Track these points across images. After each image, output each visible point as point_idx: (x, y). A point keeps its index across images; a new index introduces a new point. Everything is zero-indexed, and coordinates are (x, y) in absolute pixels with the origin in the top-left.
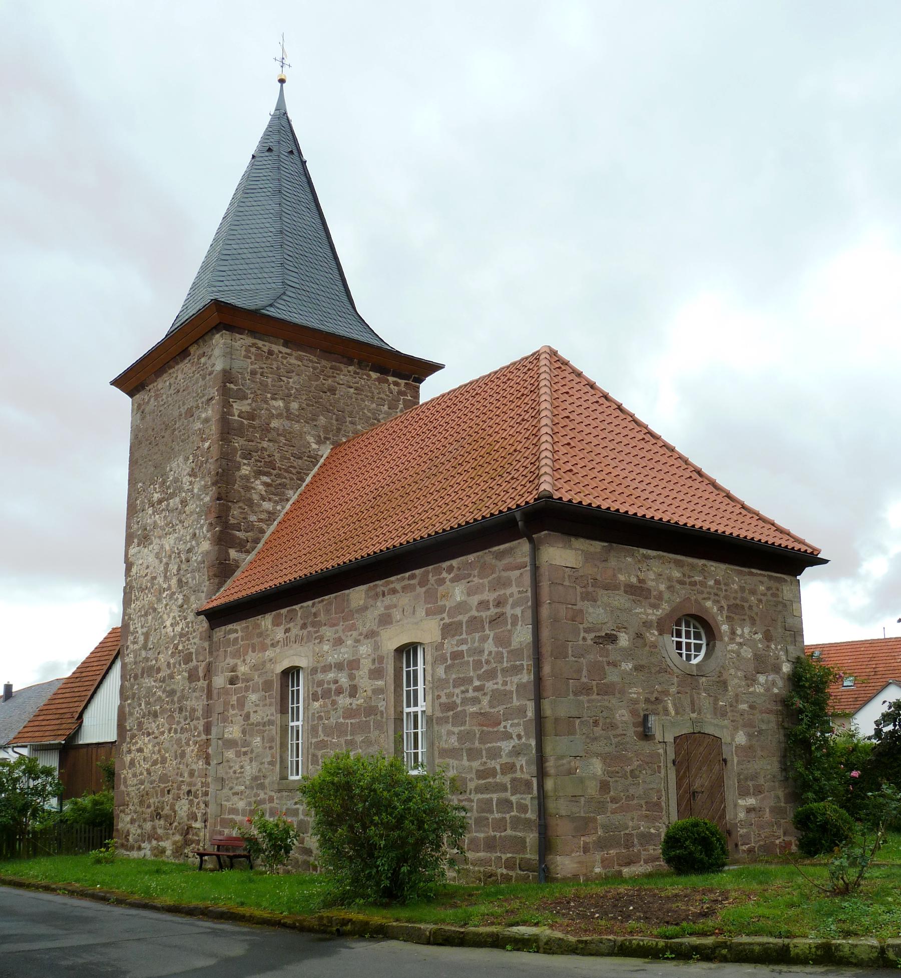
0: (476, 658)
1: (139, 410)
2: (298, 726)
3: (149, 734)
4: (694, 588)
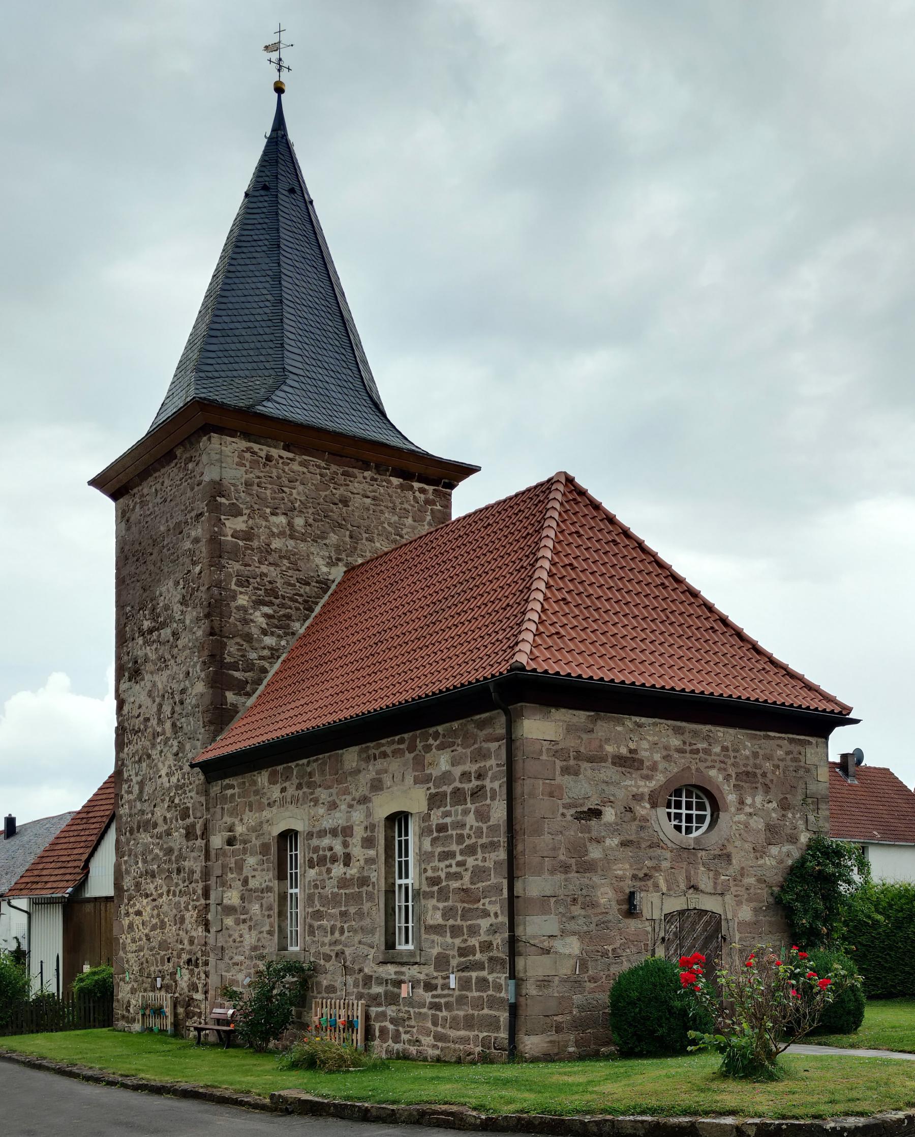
0: (459, 832)
1: (123, 517)
2: (296, 894)
3: (147, 896)
4: (696, 756)
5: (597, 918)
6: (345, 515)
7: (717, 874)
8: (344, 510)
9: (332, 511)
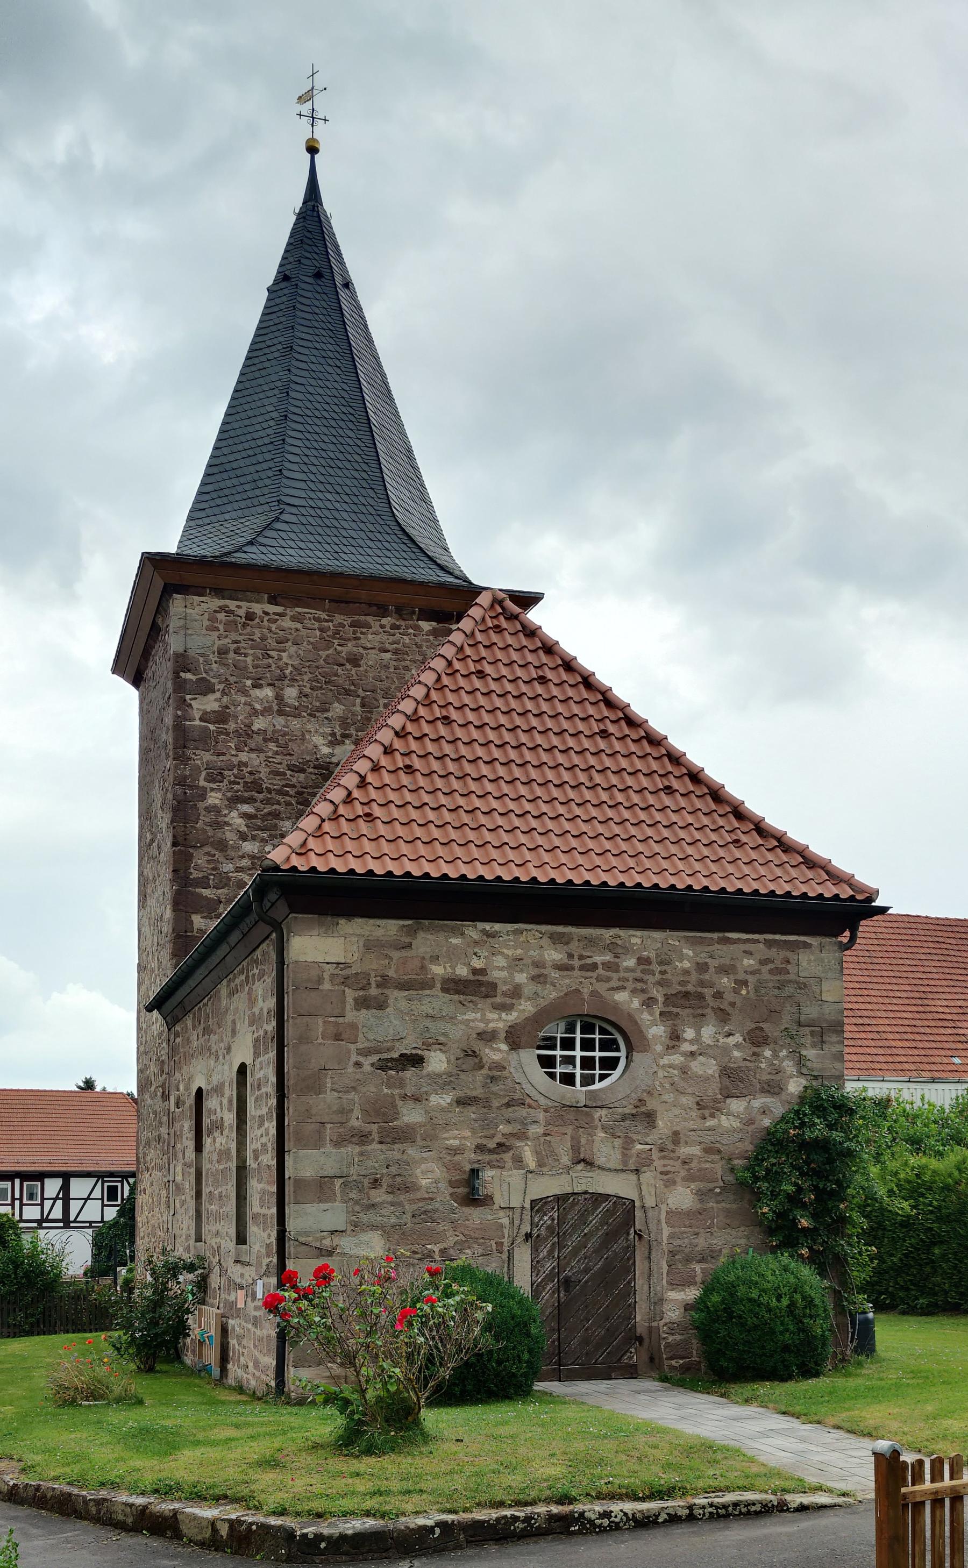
4: (589, 974)
5: (415, 1207)
6: (355, 677)
7: (628, 1143)
8: (353, 672)
9: (336, 675)
